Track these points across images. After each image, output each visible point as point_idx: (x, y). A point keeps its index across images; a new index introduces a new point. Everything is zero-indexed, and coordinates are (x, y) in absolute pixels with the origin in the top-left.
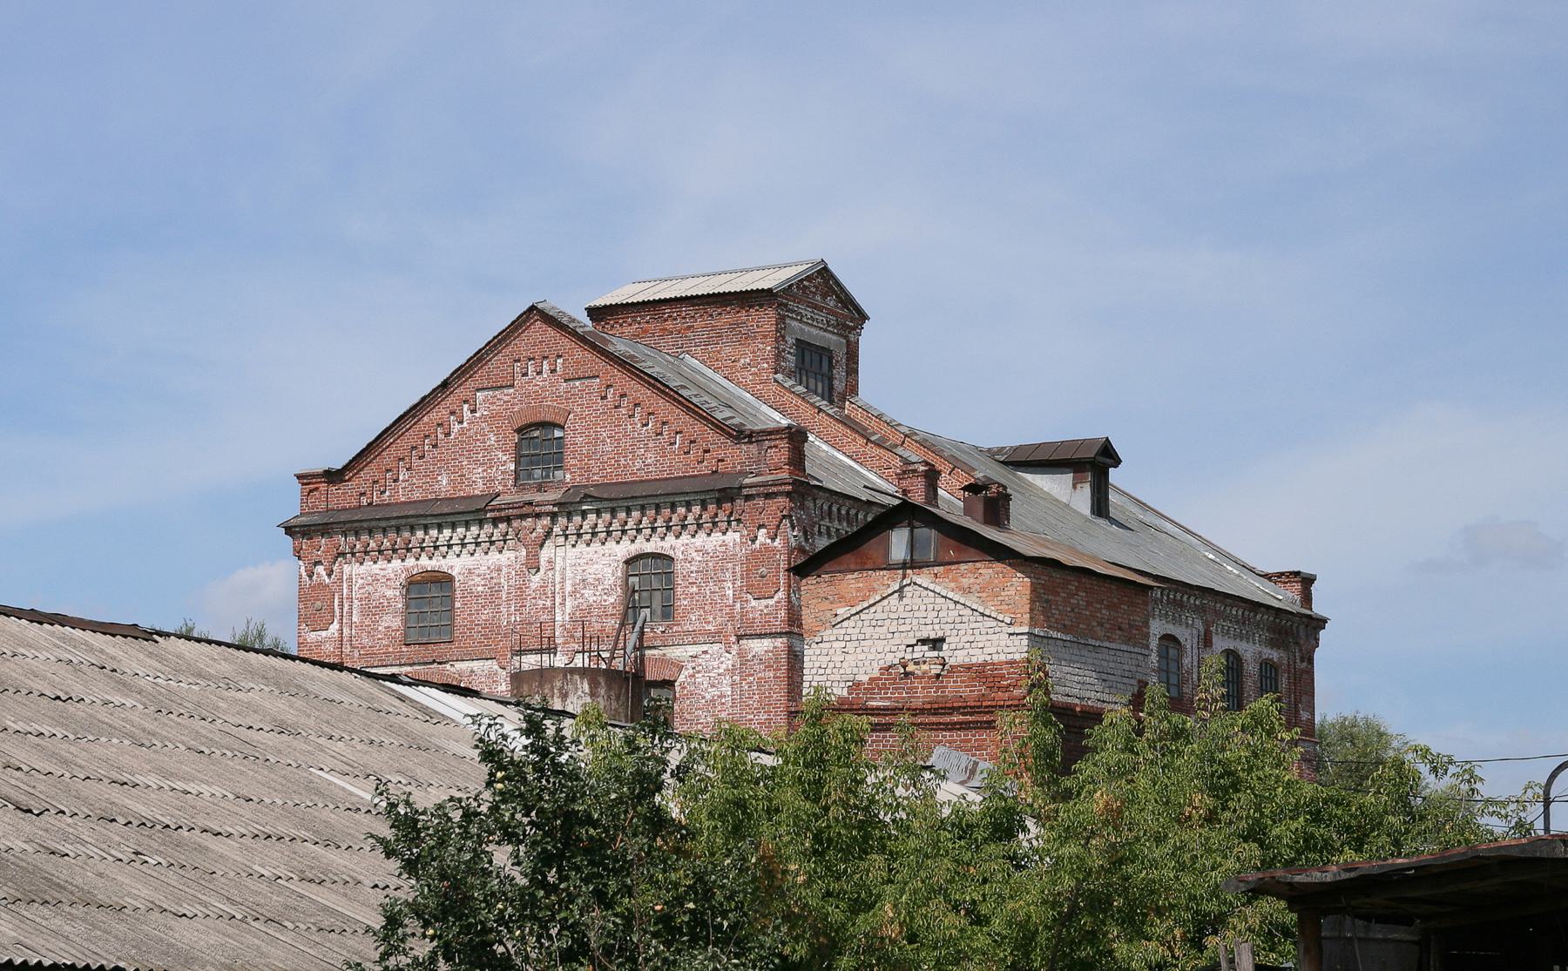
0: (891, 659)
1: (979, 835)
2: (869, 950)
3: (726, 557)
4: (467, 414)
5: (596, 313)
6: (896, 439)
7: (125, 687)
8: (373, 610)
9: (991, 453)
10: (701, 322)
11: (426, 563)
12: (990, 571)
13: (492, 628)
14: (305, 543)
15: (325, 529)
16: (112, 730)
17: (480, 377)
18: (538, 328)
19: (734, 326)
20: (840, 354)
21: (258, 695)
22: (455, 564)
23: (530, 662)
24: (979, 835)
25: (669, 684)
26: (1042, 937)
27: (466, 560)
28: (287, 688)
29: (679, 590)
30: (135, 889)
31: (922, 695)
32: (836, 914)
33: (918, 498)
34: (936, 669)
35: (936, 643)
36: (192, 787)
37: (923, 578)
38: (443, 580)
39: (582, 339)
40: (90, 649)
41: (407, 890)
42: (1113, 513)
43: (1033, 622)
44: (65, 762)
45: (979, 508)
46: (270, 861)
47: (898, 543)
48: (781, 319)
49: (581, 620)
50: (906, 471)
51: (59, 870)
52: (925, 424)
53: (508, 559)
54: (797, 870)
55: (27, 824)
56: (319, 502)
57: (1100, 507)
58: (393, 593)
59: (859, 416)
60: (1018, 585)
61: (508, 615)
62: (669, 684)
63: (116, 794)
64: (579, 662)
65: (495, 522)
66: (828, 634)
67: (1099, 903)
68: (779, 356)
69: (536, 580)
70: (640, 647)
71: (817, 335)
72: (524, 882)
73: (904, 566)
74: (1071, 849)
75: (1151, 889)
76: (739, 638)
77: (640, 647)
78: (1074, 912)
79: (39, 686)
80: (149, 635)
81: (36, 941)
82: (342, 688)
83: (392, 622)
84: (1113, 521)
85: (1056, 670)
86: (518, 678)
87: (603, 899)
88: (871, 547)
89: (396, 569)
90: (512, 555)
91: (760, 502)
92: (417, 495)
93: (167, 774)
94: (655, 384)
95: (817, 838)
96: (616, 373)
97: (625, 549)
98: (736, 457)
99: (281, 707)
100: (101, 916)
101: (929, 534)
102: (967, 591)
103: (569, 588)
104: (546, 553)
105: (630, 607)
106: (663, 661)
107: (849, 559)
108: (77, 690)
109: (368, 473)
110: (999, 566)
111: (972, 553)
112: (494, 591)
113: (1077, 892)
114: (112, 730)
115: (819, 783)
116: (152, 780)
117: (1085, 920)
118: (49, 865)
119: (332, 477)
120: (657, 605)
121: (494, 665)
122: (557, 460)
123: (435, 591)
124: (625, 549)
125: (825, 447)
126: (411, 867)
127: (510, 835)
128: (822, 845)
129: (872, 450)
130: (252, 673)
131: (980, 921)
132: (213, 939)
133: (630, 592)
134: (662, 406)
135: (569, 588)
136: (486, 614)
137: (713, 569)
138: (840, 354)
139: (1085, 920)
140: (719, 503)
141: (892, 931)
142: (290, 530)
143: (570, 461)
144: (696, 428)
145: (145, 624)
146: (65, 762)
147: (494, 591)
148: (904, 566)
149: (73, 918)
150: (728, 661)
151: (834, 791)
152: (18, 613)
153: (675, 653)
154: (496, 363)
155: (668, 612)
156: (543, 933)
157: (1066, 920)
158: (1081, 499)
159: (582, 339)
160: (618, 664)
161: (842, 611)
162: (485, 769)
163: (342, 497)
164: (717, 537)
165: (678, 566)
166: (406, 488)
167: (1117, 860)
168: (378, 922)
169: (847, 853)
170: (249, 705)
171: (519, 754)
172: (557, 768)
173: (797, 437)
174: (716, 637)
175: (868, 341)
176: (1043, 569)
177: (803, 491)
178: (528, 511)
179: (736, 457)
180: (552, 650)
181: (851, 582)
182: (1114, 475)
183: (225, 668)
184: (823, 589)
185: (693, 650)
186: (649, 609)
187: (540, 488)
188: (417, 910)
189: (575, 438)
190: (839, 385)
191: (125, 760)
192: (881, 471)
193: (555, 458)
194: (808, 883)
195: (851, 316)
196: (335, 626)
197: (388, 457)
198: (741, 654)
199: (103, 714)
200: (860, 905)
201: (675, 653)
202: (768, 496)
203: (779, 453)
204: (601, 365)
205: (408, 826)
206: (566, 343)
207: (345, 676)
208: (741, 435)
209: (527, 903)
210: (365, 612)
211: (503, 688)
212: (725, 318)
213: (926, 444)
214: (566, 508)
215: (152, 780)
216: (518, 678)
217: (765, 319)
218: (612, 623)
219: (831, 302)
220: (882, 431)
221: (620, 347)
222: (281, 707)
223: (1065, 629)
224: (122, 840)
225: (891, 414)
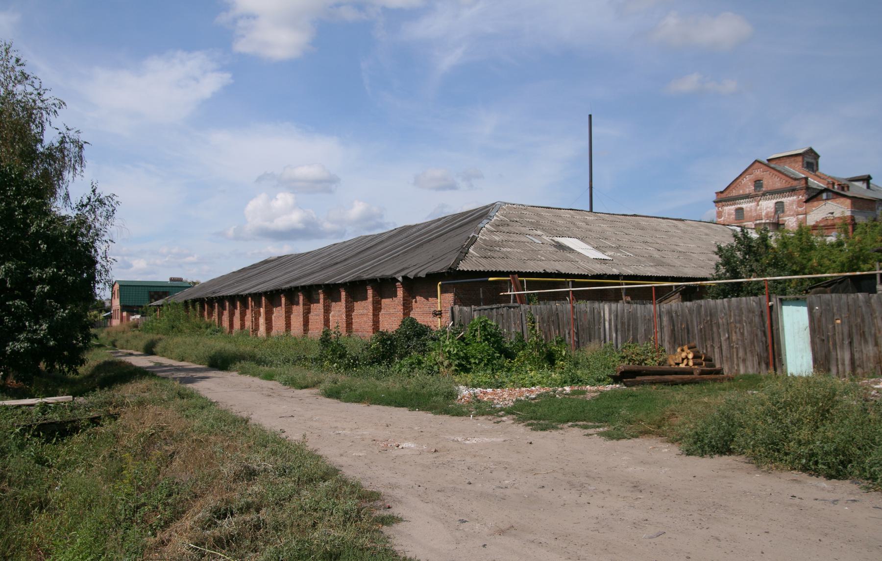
0: (824, 217)
1: (835, 246)
2: (811, 268)
3: (793, 201)
5: (769, 160)
6: (826, 178)
7: (678, 229)
8: (729, 214)
9: (846, 179)
10: (788, 160)
11: (739, 206)
12: (842, 200)
13: (751, 217)
14: (717, 204)
15: (720, 201)
16: (675, 236)
17: (747, 173)
18: (757, 164)
19: (794, 160)
20: (815, 164)
21: (703, 229)
22: (744, 206)
23: (758, 222)
24: (835, 246)
25: (783, 224)
26: (846, 265)
28: (708, 228)
30: (678, 263)
31: (830, 223)
32: (804, 262)
33: (831, 188)
34: (832, 218)
35: (832, 213)
36: (689, 245)
37: (829, 202)
38: (742, 209)
39: (765, 165)
40: (673, 223)
41: (720, 260)
42: (871, 188)
43: (852, 208)
44: (667, 242)
45: (840, 188)
46: (702, 257)
47: (824, 196)
48: (803, 158)
49: (767, 214)
50: (828, 183)
51: (664, 260)
52: (833, 175)
53: (753, 204)
54: (796, 254)
55: (659, 253)
56: (719, 197)
57: (868, 187)
58: (733, 212)
59: (819, 174)
60: (848, 202)
61: (754, 214)
62: (783, 224)
63: (675, 247)
64: (768, 221)
66: (811, 213)
67: (858, 258)
68: (803, 165)
69: (758, 208)
70: (778, 218)
71: (810, 160)
72: (742, 258)
73: (826, 200)
74: (851, 248)
75: (868, 255)
77: (778, 218)
78: (853, 260)
79: (663, 230)
80: (683, 220)
81: (660, 272)
82: (718, 227)
83: (733, 216)
84: (871, 190)
85: (856, 217)
86: (756, 225)
87: (757, 261)
88: (819, 197)
89: (733, 207)
92: (737, 194)
93: (684, 243)
94: (779, 172)
95: (801, 248)
96: (772, 170)
97: (775, 201)
98: (795, 183)
99: (707, 231)
100: (671, 267)
101: (830, 194)
102: (838, 203)
104: (760, 203)
105: (776, 211)
106: (783, 220)
107: (815, 199)
108: (670, 230)
109: (727, 192)
112: (751, 210)
113: (853, 256)
114: (675, 236)
115: (801, 238)
116: (682, 244)
117: (855, 261)
118: (662, 259)
119: (721, 192)
120: (781, 210)
121: (751, 223)
123: (740, 211)
124: (775, 201)
125: (812, 180)
126: (720, 256)
127: (739, 250)
128: (802, 249)
129: (821, 180)
130: (702, 226)
131: (834, 262)
132: (691, 271)
133: (776, 208)
136: (750, 214)
137: (792, 203)
138: (815, 164)
139: (855, 261)
140: (792, 191)
141: (815, 264)
142: (714, 202)
143: (764, 186)
144: (787, 179)
145: (683, 218)
146: (667, 242)
147: (751, 210)
148: (826, 200)
149: (665, 268)
150: (795, 219)
151: (804, 240)
152: (660, 218)
153: (785, 219)
154: (750, 170)
155: (783, 212)
156: (745, 267)
157: (851, 261)
158: (864, 186)
159: (765, 165)
160: (774, 221)
161: (814, 209)
162: (734, 238)
163: (723, 196)
164: (792, 198)
165: (785, 204)
166: (734, 193)
167: (861, 250)
168: (715, 267)
169: (807, 251)
170: (701, 231)
171: (740, 236)
172: (747, 238)
173: (806, 179)
174: (792, 215)
175: (820, 161)
176: (853, 198)
177: (808, 188)
178: (757, 196)
179: (795, 183)
180: (762, 219)
181: (815, 203)
182: (871, 181)
183: (696, 225)
185: (788, 218)
186: (589, 210)
187: (759, 191)
188: (721, 264)
189: (765, 182)
190: (815, 169)
191: (678, 241)
192: (823, 183)
193: (761, 186)
194: (799, 256)
195: (817, 156)
196: (723, 218)
197: (731, 188)
198: (797, 218)
199: (674, 234)
200: (810, 260)
201: (785, 219)
203: (803, 182)
204: (769, 169)
205: (720, 249)
206: (762, 166)
207: (719, 225)
208: (796, 179)
209: (742, 262)
210: (728, 215)
211: (753, 227)
212: (793, 159)
213: (832, 178)
214: (764, 195)
215: (682, 244)
216: (756, 225)
217: (800, 159)
218: (773, 214)
219: (813, 154)
220: (823, 177)
221: (772, 165)
222: (707, 231)
223: (858, 209)
224: (676, 255)
225: (825, 173)
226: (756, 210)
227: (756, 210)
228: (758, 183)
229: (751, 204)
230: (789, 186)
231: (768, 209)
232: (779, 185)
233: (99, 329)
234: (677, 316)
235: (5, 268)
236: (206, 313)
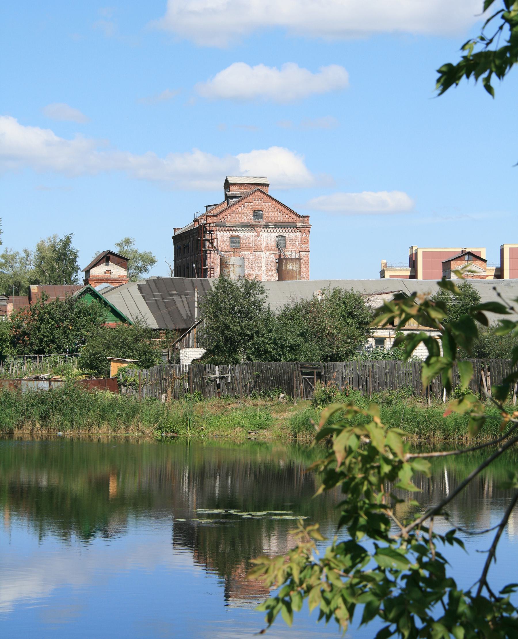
4: (243, 207)
8: (223, 241)
27: (243, 233)
29: (287, 243)
38: (238, 237)
58: (228, 238)
65: (251, 227)
69: (259, 238)
76: (300, 252)
88: (462, 258)
90: (253, 233)
91: (305, 229)
97: (276, 234)
102: (477, 265)
103: (265, 240)
104: (261, 234)
107: (459, 259)
109: (222, 215)
110: (482, 262)
111: (478, 260)
112: (249, 240)
122: (262, 217)
124: (276, 234)
134: (284, 209)
135: (265, 240)
136: (247, 244)
165: (287, 238)
184: (455, 263)
189: (266, 214)
202: (306, 228)
226: (255, 241)
227: (255, 241)
228: (258, 214)
229: (249, 234)
230: (292, 221)
231: (269, 242)
232: (281, 219)
233: (305, 581)
234: (107, 326)
235: (104, 350)
236: (300, 468)
